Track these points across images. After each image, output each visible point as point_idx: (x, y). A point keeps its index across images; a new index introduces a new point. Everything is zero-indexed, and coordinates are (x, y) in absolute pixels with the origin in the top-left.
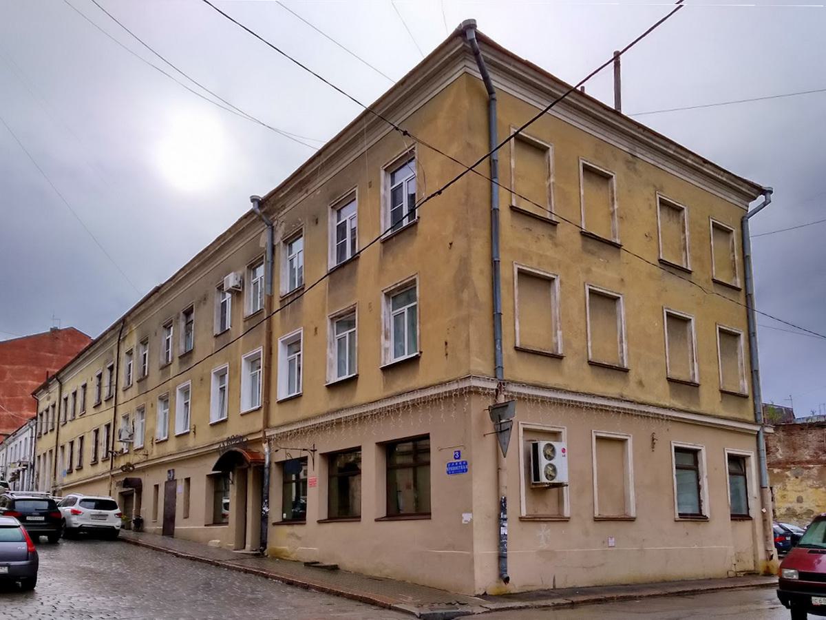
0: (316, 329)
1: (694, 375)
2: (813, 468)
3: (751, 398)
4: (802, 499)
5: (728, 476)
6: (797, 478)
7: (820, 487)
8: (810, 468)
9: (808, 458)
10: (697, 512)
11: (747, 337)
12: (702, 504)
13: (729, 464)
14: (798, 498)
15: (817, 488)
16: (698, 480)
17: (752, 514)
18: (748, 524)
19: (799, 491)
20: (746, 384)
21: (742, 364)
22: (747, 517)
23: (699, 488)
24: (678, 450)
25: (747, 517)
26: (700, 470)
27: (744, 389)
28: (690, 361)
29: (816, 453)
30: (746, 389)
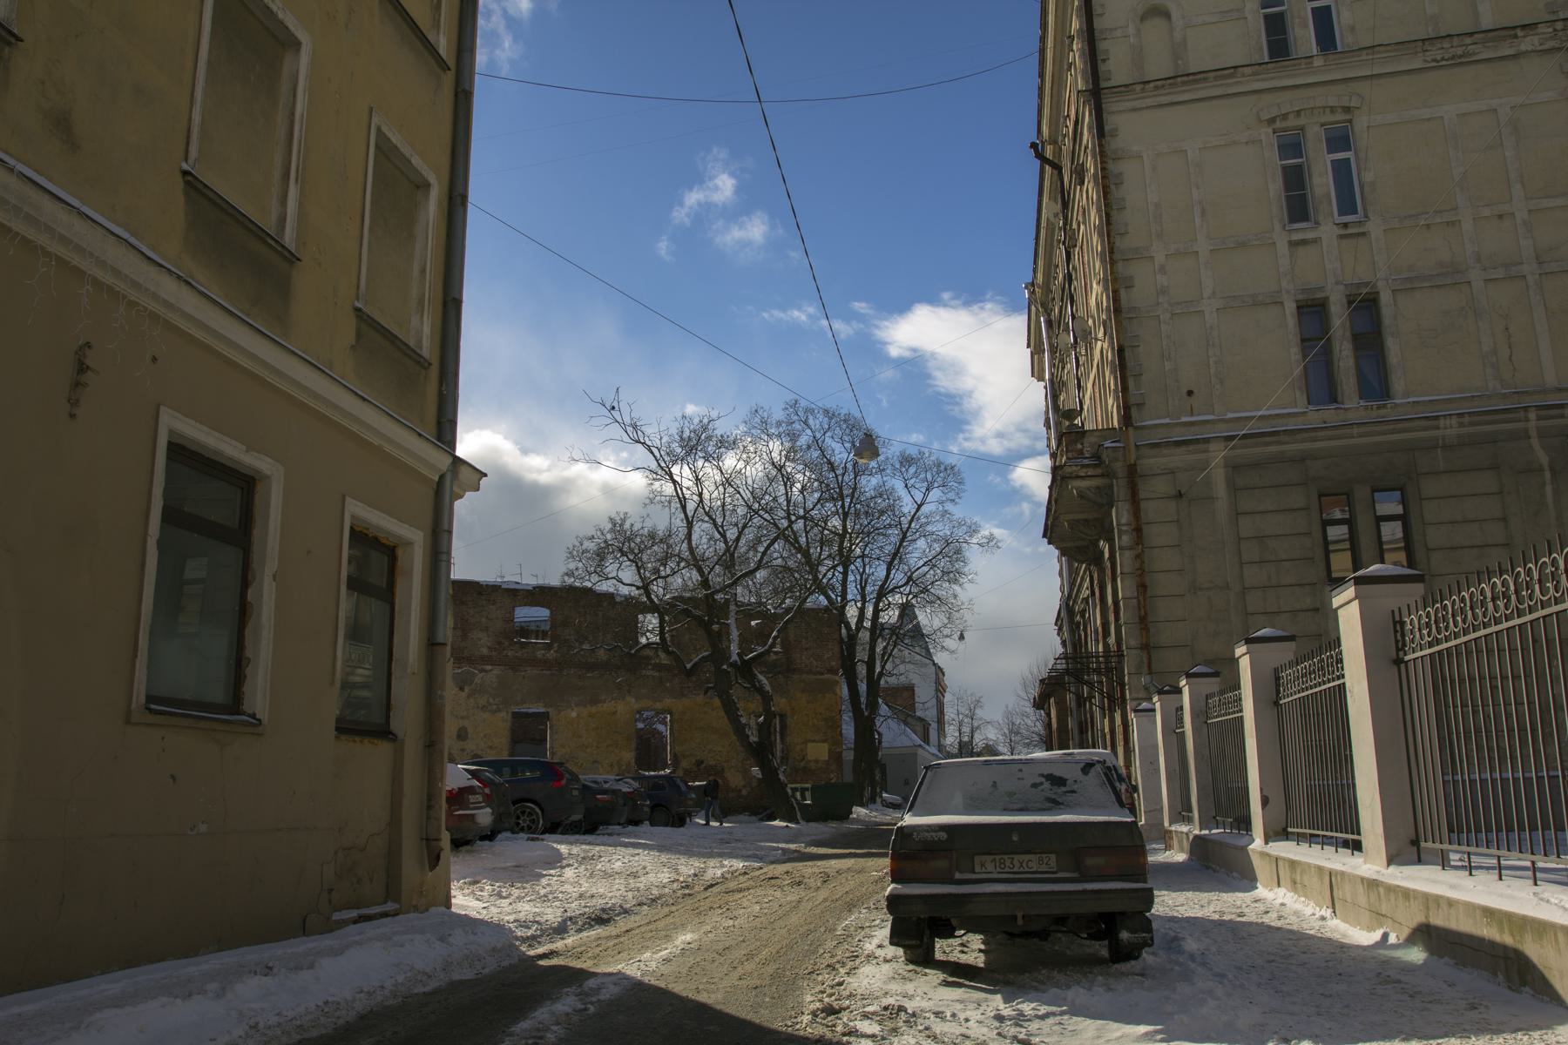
0: (211, 1040)
1: (282, 220)
2: (491, 670)
3: (434, 372)
4: (466, 732)
5: (344, 588)
6: (462, 689)
7: (499, 710)
8: (486, 671)
9: (485, 651)
10: (217, 694)
11: (445, 204)
12: (248, 671)
13: (351, 547)
14: (460, 730)
15: (494, 712)
16: (245, 584)
17: (395, 726)
18: (383, 748)
19: (462, 718)
20: (427, 330)
21: (423, 271)
22: (383, 732)
23: (244, 612)
24: (179, 452)
25: (383, 732)
26: (256, 548)
27: (420, 341)
28: (277, 174)
29: (499, 643)
30: (426, 343)
